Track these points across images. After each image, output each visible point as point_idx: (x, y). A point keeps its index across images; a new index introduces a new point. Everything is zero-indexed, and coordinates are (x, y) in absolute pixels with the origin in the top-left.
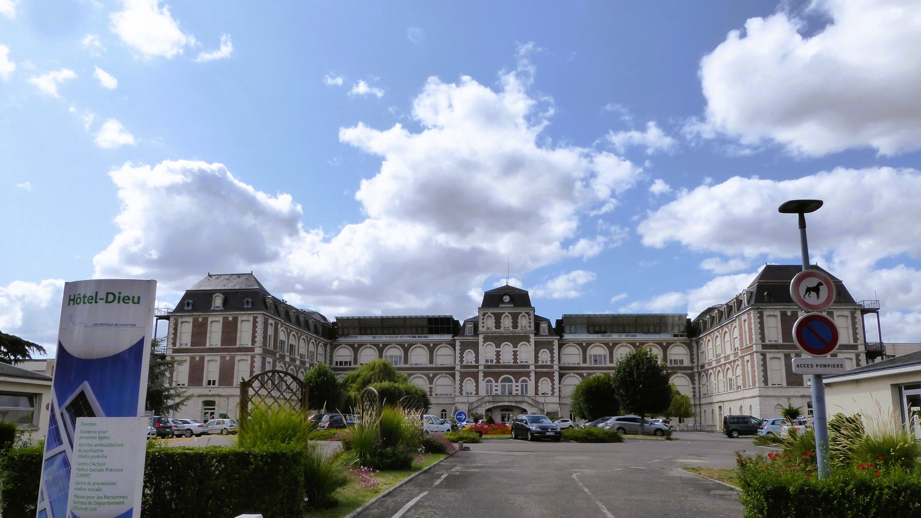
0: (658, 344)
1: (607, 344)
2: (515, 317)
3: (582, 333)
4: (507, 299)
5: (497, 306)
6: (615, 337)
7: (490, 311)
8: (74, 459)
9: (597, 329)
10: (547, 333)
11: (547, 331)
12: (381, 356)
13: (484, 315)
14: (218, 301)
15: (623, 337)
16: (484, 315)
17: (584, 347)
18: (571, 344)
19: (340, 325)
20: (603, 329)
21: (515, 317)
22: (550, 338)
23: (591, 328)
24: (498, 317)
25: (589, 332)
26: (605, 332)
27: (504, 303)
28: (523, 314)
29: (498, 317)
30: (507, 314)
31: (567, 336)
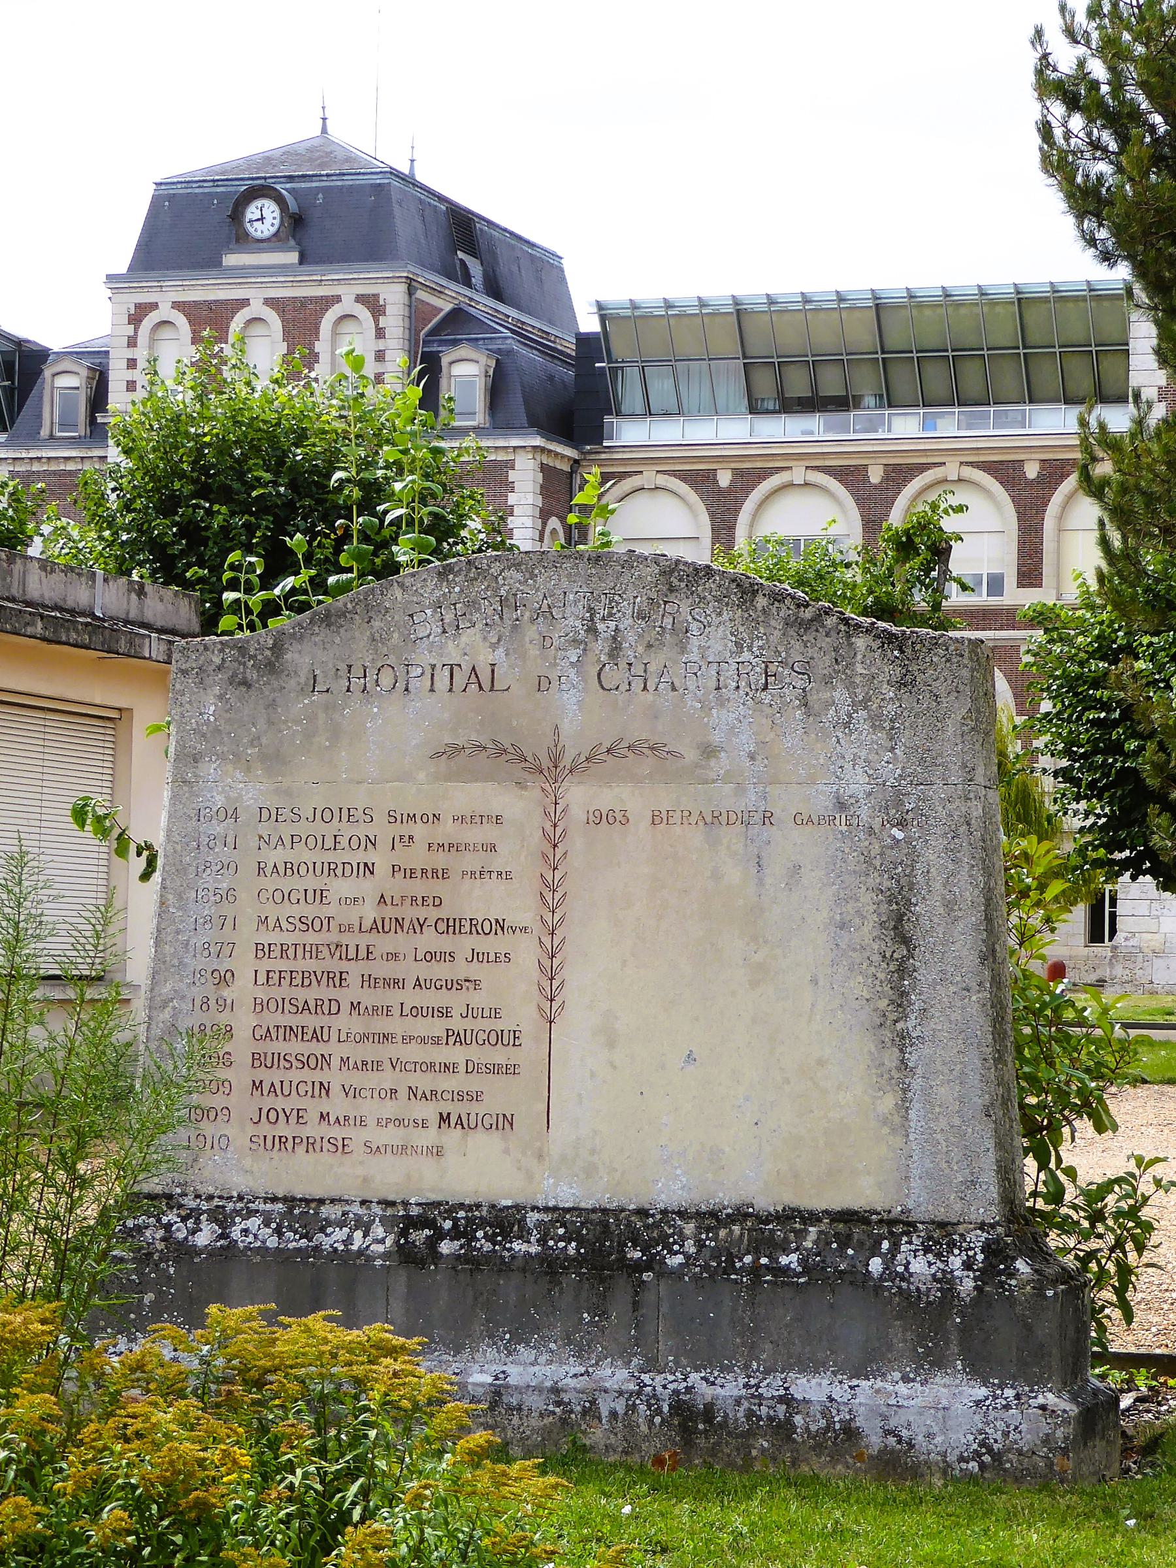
0: (988, 467)
1: (850, 475)
2: (302, 322)
3: (716, 411)
4: (264, 217)
5: (206, 261)
6: (905, 427)
7: (168, 294)
8: (662, 1206)
9: (798, 385)
10: (480, 418)
11: (479, 401)
12: (723, 531)
13: (136, 319)
14: (264, 217)
15: (950, 425)
16: (136, 319)
17: (723, 491)
18: (649, 477)
19: (620, 349)
20: (831, 385)
21: (302, 322)
22: (497, 446)
23: (765, 383)
24: (210, 320)
25: (755, 408)
26: (843, 403)
27: (242, 239)
28: (348, 305)
29: (210, 320)
30: (257, 308)
31: (629, 433)
